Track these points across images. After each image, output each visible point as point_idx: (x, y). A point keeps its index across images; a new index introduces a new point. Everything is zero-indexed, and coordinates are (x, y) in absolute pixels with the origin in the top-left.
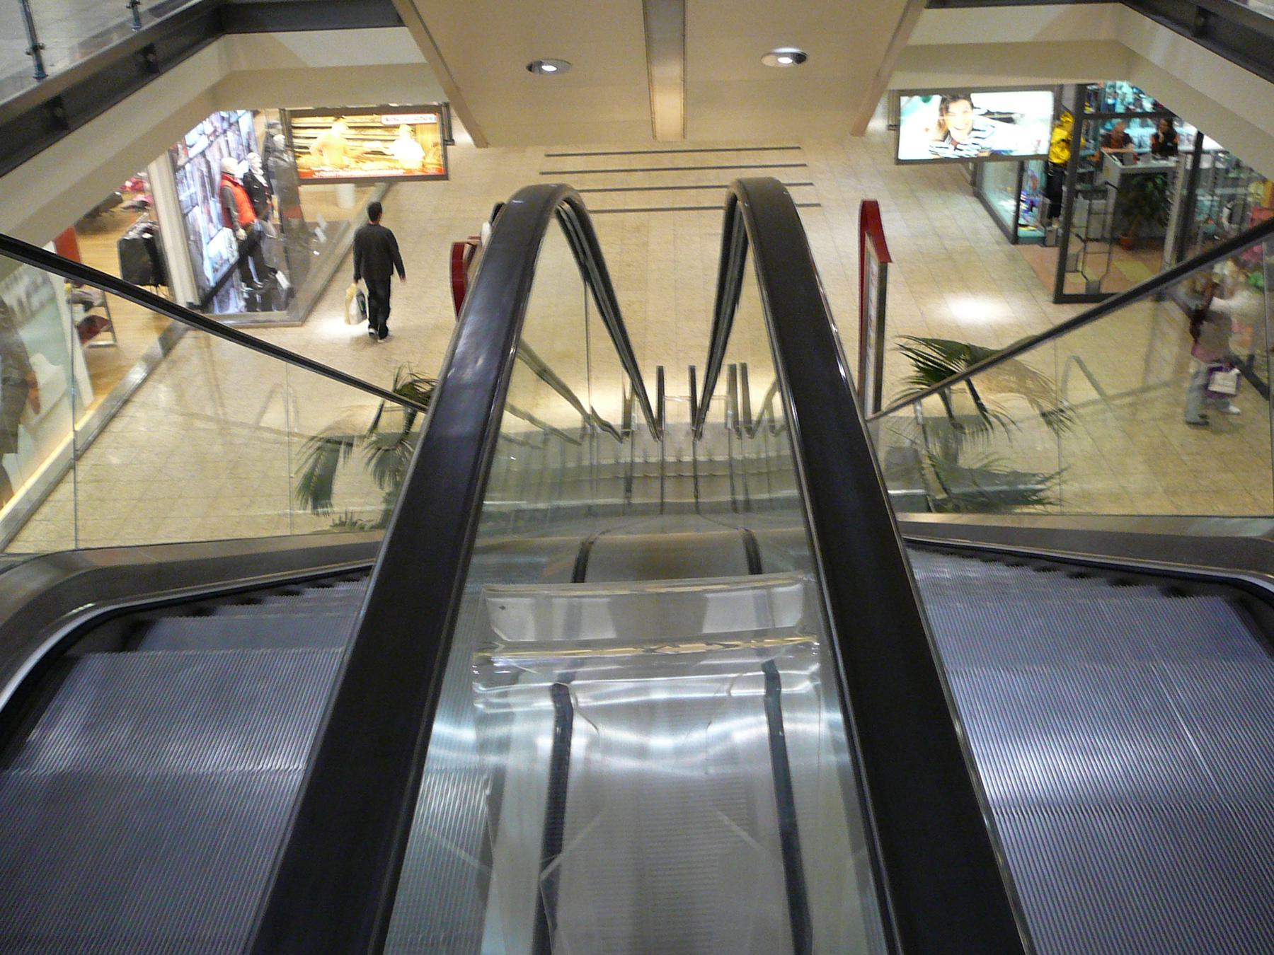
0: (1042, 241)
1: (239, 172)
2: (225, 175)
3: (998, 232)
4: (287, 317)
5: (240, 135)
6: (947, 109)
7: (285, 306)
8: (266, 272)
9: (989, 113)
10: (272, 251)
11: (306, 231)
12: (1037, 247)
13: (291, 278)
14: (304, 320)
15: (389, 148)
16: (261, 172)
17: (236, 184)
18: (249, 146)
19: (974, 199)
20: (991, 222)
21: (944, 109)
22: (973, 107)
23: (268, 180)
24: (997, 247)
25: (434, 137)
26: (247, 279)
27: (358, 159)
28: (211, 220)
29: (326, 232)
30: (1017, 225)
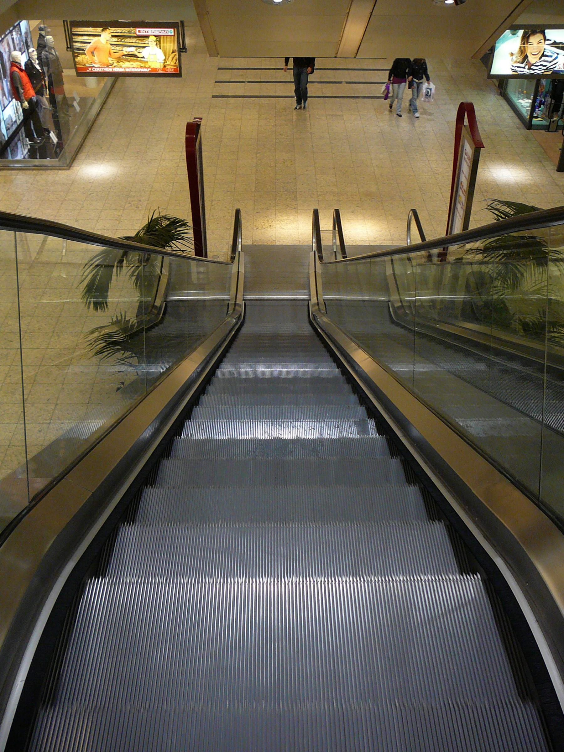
0: (547, 128)
1: (22, 59)
2: (14, 63)
3: (517, 120)
4: (58, 164)
5: (21, 34)
6: (528, 38)
7: (56, 155)
8: (43, 132)
9: (555, 43)
10: (46, 120)
11: (67, 103)
12: (543, 132)
13: (59, 136)
14: (69, 166)
15: (144, 53)
16: (37, 62)
17: (21, 70)
18: (27, 42)
19: (500, 97)
20: (512, 114)
21: (525, 39)
22: (545, 39)
23: (42, 69)
24: (518, 131)
25: (171, 46)
26: (29, 135)
27: (119, 60)
28: (4, 94)
29: (79, 104)
30: (532, 117)
